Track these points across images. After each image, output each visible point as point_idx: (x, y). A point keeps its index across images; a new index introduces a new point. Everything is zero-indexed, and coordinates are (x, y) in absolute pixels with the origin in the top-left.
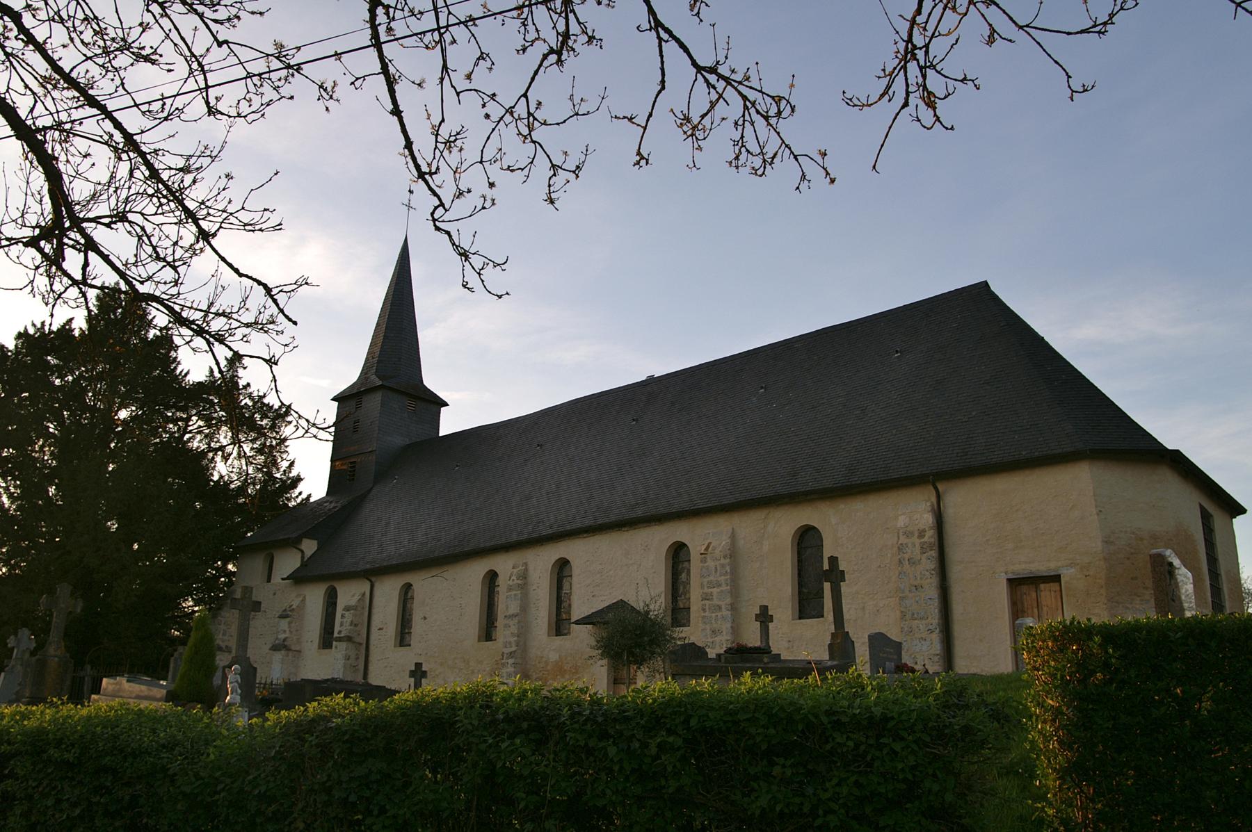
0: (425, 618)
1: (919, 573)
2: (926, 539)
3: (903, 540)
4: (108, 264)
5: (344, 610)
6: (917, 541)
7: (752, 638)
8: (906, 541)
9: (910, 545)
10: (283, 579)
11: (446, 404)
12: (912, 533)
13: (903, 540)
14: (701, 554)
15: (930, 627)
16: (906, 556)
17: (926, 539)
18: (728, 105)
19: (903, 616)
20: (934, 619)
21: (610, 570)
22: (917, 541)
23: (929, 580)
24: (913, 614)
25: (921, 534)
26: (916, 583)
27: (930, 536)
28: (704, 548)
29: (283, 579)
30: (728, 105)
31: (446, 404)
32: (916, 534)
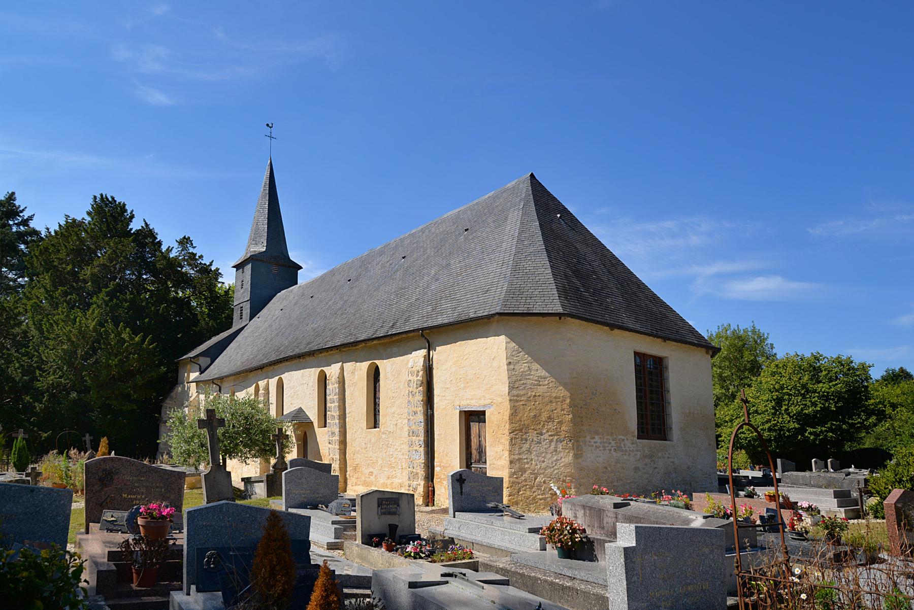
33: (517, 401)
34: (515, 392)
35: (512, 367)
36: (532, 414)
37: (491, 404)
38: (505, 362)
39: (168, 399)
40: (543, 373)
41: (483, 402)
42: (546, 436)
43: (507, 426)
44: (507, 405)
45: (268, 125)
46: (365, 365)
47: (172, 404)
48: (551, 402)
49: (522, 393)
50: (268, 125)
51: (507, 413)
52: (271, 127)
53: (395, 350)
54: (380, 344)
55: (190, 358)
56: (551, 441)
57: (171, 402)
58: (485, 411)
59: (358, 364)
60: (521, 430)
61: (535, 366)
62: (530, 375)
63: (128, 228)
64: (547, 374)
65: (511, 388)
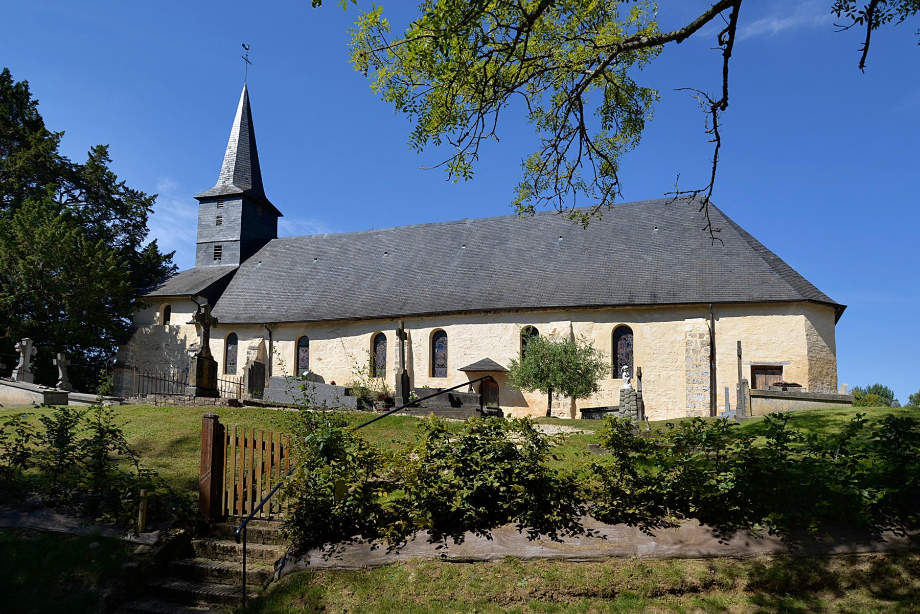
0: (320, 359)
1: (699, 357)
2: (705, 339)
3: (689, 338)
4: (252, 123)
5: (249, 349)
6: (699, 340)
7: (712, 105)
8: (691, 339)
9: (693, 342)
10: (187, 323)
11: (281, 215)
12: (695, 335)
13: (689, 338)
14: (550, 335)
15: (705, 388)
16: (691, 348)
17: (705, 339)
18: (739, 343)
19: (688, 381)
20: (708, 385)
21: (478, 339)
22: (699, 340)
23: (705, 363)
24: (694, 381)
25: (701, 336)
26: (697, 363)
27: (707, 338)
28: (552, 330)
29: (187, 323)
30: (739, 343)
31: (281, 215)
32: (698, 336)
33: (812, 360)
34: (811, 354)
35: (808, 337)
36: (819, 370)
37: (787, 363)
38: (805, 334)
39: (131, 340)
40: (824, 344)
41: (782, 360)
42: (825, 385)
43: (807, 377)
44: (807, 362)
45: (244, 45)
46: (609, 327)
47: (135, 346)
48: (828, 363)
49: (814, 355)
50: (244, 45)
51: (807, 367)
52: (247, 49)
53: (656, 316)
54: (631, 309)
55: (192, 295)
56: (828, 389)
57: (134, 345)
58: (782, 367)
59: (597, 324)
60: (813, 380)
61: (820, 339)
62: (817, 344)
63: (28, 101)
64: (826, 345)
65: (809, 351)
